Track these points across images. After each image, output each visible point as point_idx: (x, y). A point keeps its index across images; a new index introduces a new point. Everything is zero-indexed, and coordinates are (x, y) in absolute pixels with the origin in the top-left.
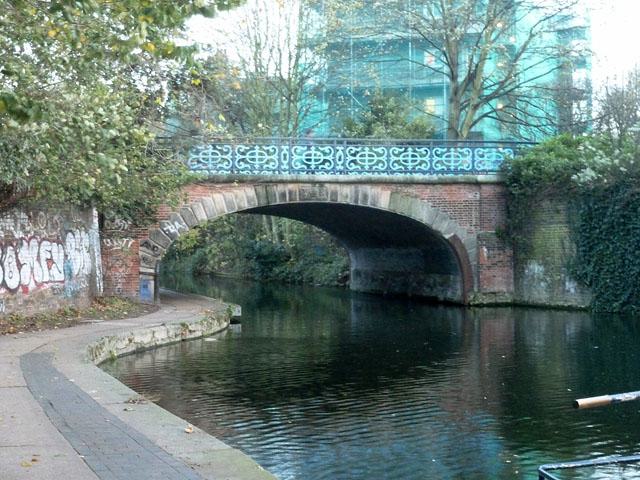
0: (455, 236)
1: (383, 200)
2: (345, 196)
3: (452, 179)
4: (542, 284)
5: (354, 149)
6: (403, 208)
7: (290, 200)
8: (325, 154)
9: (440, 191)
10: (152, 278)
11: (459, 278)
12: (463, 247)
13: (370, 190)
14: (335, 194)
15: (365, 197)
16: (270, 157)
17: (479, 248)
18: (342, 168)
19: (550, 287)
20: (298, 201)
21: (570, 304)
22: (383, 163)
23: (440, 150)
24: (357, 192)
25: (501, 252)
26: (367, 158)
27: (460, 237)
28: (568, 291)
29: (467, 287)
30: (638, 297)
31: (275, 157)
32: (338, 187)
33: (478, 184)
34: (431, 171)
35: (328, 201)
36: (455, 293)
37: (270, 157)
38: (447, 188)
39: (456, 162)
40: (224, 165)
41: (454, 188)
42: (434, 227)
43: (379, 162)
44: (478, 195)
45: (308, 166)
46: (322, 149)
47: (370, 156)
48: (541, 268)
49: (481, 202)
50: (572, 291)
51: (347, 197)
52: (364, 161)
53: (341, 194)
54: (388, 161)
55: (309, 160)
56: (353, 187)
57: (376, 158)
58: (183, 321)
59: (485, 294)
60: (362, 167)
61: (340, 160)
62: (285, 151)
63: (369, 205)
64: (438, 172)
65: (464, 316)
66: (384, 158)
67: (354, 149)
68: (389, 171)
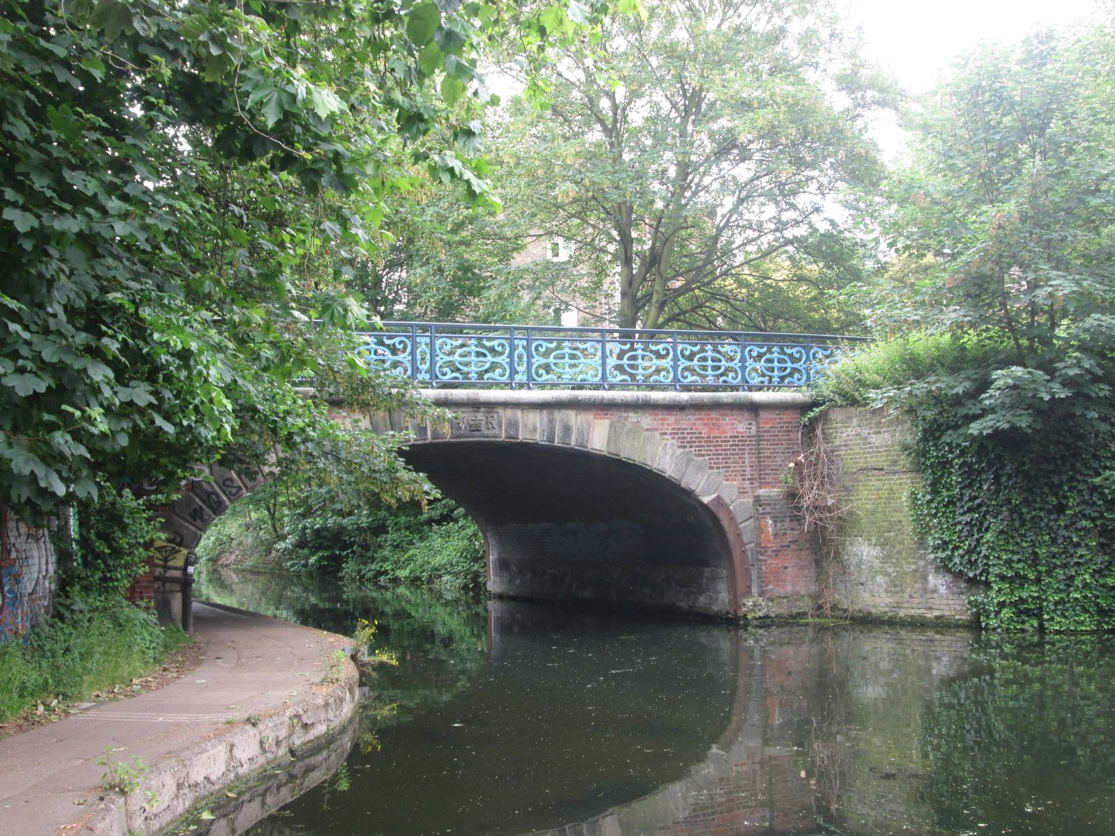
0: (719, 498)
3: (464, 397)
6: (631, 451)
7: (433, 438)
8: (394, 351)
9: (688, 421)
10: (177, 587)
11: (724, 573)
13: (574, 418)
14: (513, 425)
15: (567, 430)
16: (450, 358)
17: (758, 518)
19: (896, 586)
21: (937, 613)
22: (502, 366)
24: (551, 421)
25: (795, 523)
27: (728, 501)
28: (934, 591)
29: (741, 587)
31: (503, 360)
32: (519, 413)
33: (754, 408)
34: (676, 385)
35: (503, 437)
36: (721, 599)
37: (450, 358)
38: (703, 415)
39: (780, 369)
41: (714, 415)
44: (754, 428)
46: (654, 348)
47: (780, 361)
49: (759, 437)
50: (943, 590)
51: (535, 429)
53: (525, 426)
55: (573, 357)
56: (545, 412)
59: (771, 600)
60: (633, 376)
63: (573, 443)
64: (687, 388)
65: (737, 642)
66: (736, 364)
67: (689, 349)
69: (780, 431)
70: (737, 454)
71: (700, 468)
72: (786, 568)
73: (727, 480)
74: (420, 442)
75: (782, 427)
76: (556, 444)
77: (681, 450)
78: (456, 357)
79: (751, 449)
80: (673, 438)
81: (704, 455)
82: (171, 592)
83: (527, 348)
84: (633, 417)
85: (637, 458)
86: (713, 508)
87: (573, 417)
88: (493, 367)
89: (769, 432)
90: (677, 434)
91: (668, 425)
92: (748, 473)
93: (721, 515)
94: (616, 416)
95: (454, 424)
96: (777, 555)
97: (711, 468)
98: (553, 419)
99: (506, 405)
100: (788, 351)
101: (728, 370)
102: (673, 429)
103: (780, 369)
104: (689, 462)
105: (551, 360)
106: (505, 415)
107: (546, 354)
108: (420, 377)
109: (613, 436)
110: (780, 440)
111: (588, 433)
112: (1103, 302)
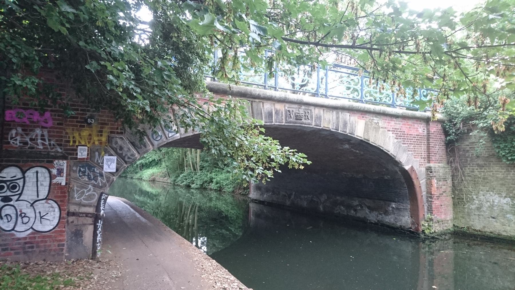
10: (90, 220)
14: (319, 118)
15: (345, 124)
24: (338, 118)
35: (313, 125)
51: (329, 122)
56: (335, 112)
69: (437, 134)
70: (419, 144)
71: (404, 151)
72: (441, 205)
73: (415, 158)
74: (268, 124)
75: (438, 132)
76: (339, 131)
77: (397, 140)
79: (424, 142)
80: (393, 133)
81: (405, 144)
82: (84, 225)
84: (376, 120)
86: (410, 172)
87: (347, 115)
89: (433, 134)
90: (395, 131)
91: (391, 126)
93: (413, 176)
94: (369, 117)
96: (438, 199)
97: (409, 151)
98: (339, 117)
99: (316, 105)
100: (372, 98)
102: (393, 128)
104: (400, 146)
109: (366, 130)
110: (437, 138)
111: (355, 127)
112: (375, 100)
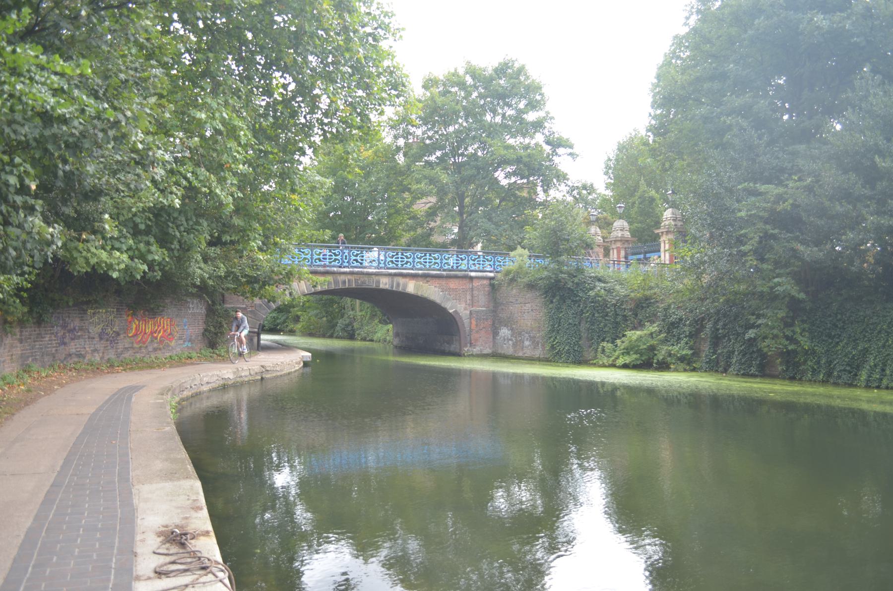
0: (456, 311)
1: (411, 287)
2: (384, 283)
4: (510, 342)
5: (392, 254)
12: (461, 318)
13: (402, 280)
14: (378, 282)
15: (398, 285)
18: (347, 264)
20: (354, 286)
23: (447, 256)
24: (393, 282)
26: (400, 259)
30: (888, 333)
35: (374, 286)
40: (336, 263)
42: (443, 305)
43: (407, 262)
45: (397, 265)
48: (510, 332)
52: (430, 259)
54: (441, 263)
57: (406, 260)
58: (263, 364)
61: (346, 259)
62: (346, 254)
63: (400, 289)
64: (444, 270)
68: (377, 267)
78: (422, 260)
83: (349, 253)
85: (426, 295)
88: (407, 262)
92: (468, 301)
95: (336, 282)
101: (336, 260)
103: (401, 261)
105: (476, 262)
106: (375, 278)
107: (357, 255)
108: (381, 265)
109: (416, 287)
